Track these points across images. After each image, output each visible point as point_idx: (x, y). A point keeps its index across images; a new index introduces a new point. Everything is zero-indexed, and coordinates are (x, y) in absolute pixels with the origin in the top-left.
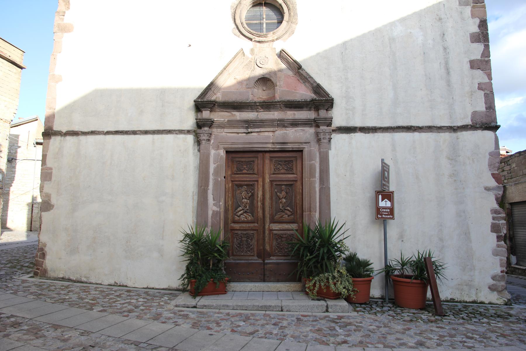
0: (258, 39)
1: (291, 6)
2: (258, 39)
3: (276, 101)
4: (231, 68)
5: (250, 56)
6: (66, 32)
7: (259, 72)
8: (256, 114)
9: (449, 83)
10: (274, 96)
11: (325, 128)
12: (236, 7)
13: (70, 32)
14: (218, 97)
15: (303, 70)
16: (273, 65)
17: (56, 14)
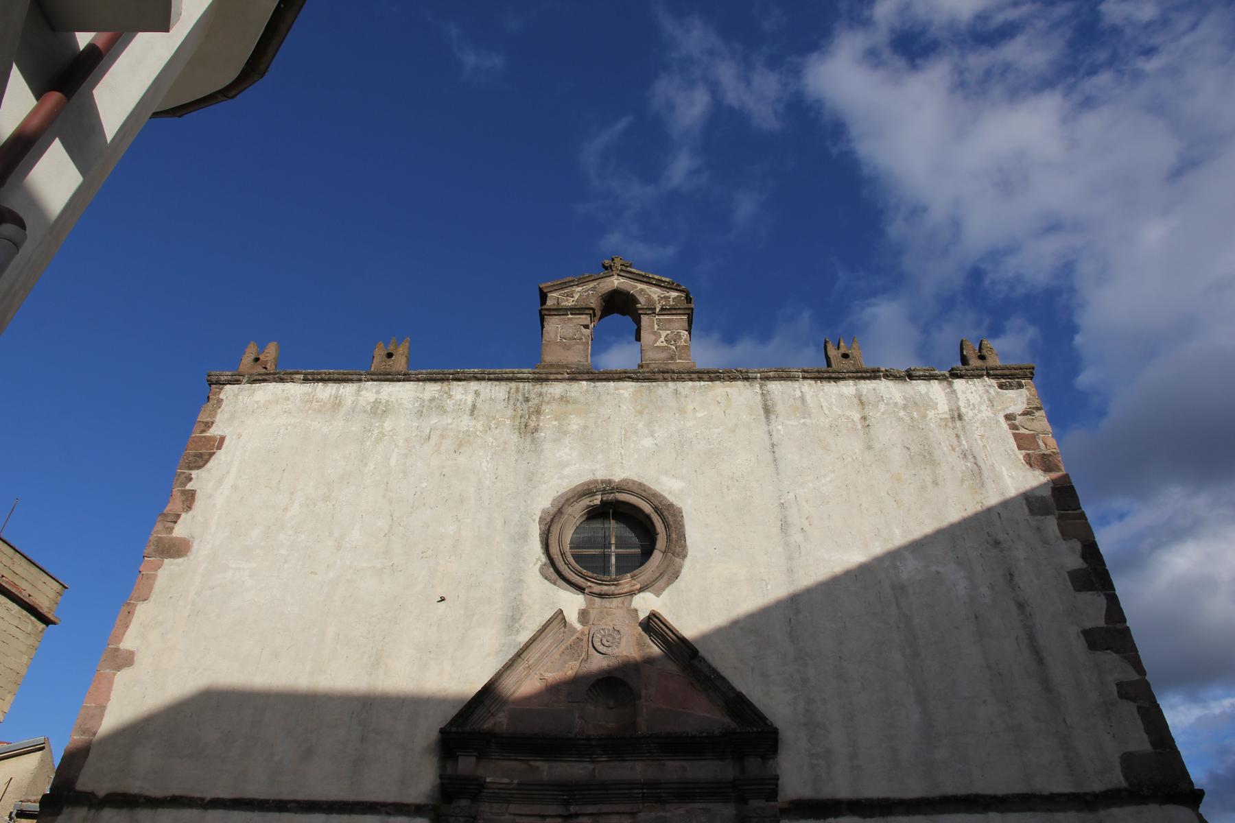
0: (596, 589)
1: (671, 519)
2: (596, 589)
4: (533, 655)
5: (579, 627)
6: (171, 557)
8: (591, 766)
9: (1046, 684)
11: (760, 803)
12: (552, 520)
13: (179, 556)
14: (499, 721)
15: (702, 660)
16: (630, 646)
17: (160, 518)
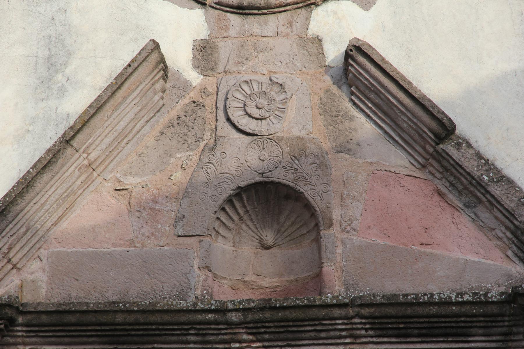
3: (329, 298)
4: (97, 140)
5: (194, 77)
7: (241, 160)
10: (319, 276)
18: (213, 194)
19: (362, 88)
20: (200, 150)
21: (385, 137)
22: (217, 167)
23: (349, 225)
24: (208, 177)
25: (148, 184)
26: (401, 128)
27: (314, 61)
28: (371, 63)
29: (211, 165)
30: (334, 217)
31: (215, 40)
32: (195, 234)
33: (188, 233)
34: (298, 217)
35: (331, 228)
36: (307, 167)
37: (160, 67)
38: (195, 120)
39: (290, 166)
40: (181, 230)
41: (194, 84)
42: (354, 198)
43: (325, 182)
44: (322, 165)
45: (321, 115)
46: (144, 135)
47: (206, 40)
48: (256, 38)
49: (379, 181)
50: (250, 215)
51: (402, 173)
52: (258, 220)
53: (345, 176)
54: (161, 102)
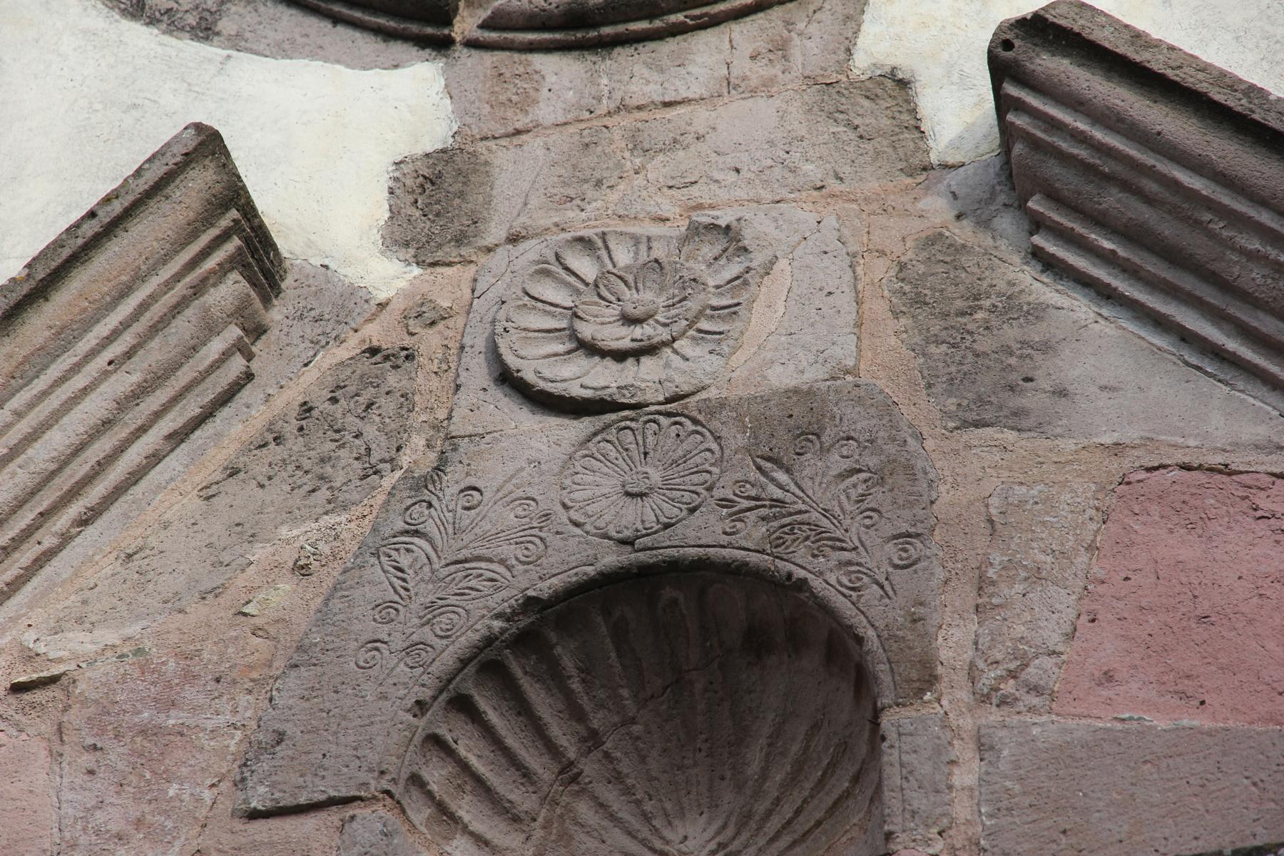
5: (389, 276)
7: (551, 505)
18: (415, 638)
19: (1066, 179)
20: (380, 498)
21: (1181, 358)
22: (439, 543)
23: (1012, 674)
24: (398, 583)
25: (147, 644)
26: (1245, 297)
27: (878, 154)
28: (1089, 67)
29: (416, 540)
30: (944, 654)
31: (481, 147)
32: (323, 797)
33: (294, 795)
34: (816, 727)
35: (928, 696)
36: (819, 483)
37: (225, 222)
38: (369, 406)
39: (753, 493)
40: (262, 790)
41: (382, 296)
42: (1037, 575)
43: (905, 527)
44: (890, 472)
45: (896, 315)
46: (160, 488)
47: (444, 151)
48: (643, 115)
49: (1155, 509)
50: (607, 755)
51: (1260, 468)
52: (651, 779)
53: (995, 501)
54: (237, 365)
